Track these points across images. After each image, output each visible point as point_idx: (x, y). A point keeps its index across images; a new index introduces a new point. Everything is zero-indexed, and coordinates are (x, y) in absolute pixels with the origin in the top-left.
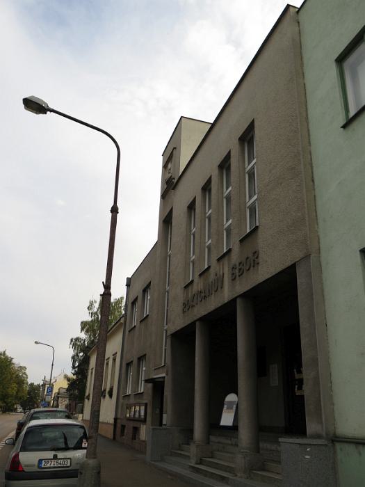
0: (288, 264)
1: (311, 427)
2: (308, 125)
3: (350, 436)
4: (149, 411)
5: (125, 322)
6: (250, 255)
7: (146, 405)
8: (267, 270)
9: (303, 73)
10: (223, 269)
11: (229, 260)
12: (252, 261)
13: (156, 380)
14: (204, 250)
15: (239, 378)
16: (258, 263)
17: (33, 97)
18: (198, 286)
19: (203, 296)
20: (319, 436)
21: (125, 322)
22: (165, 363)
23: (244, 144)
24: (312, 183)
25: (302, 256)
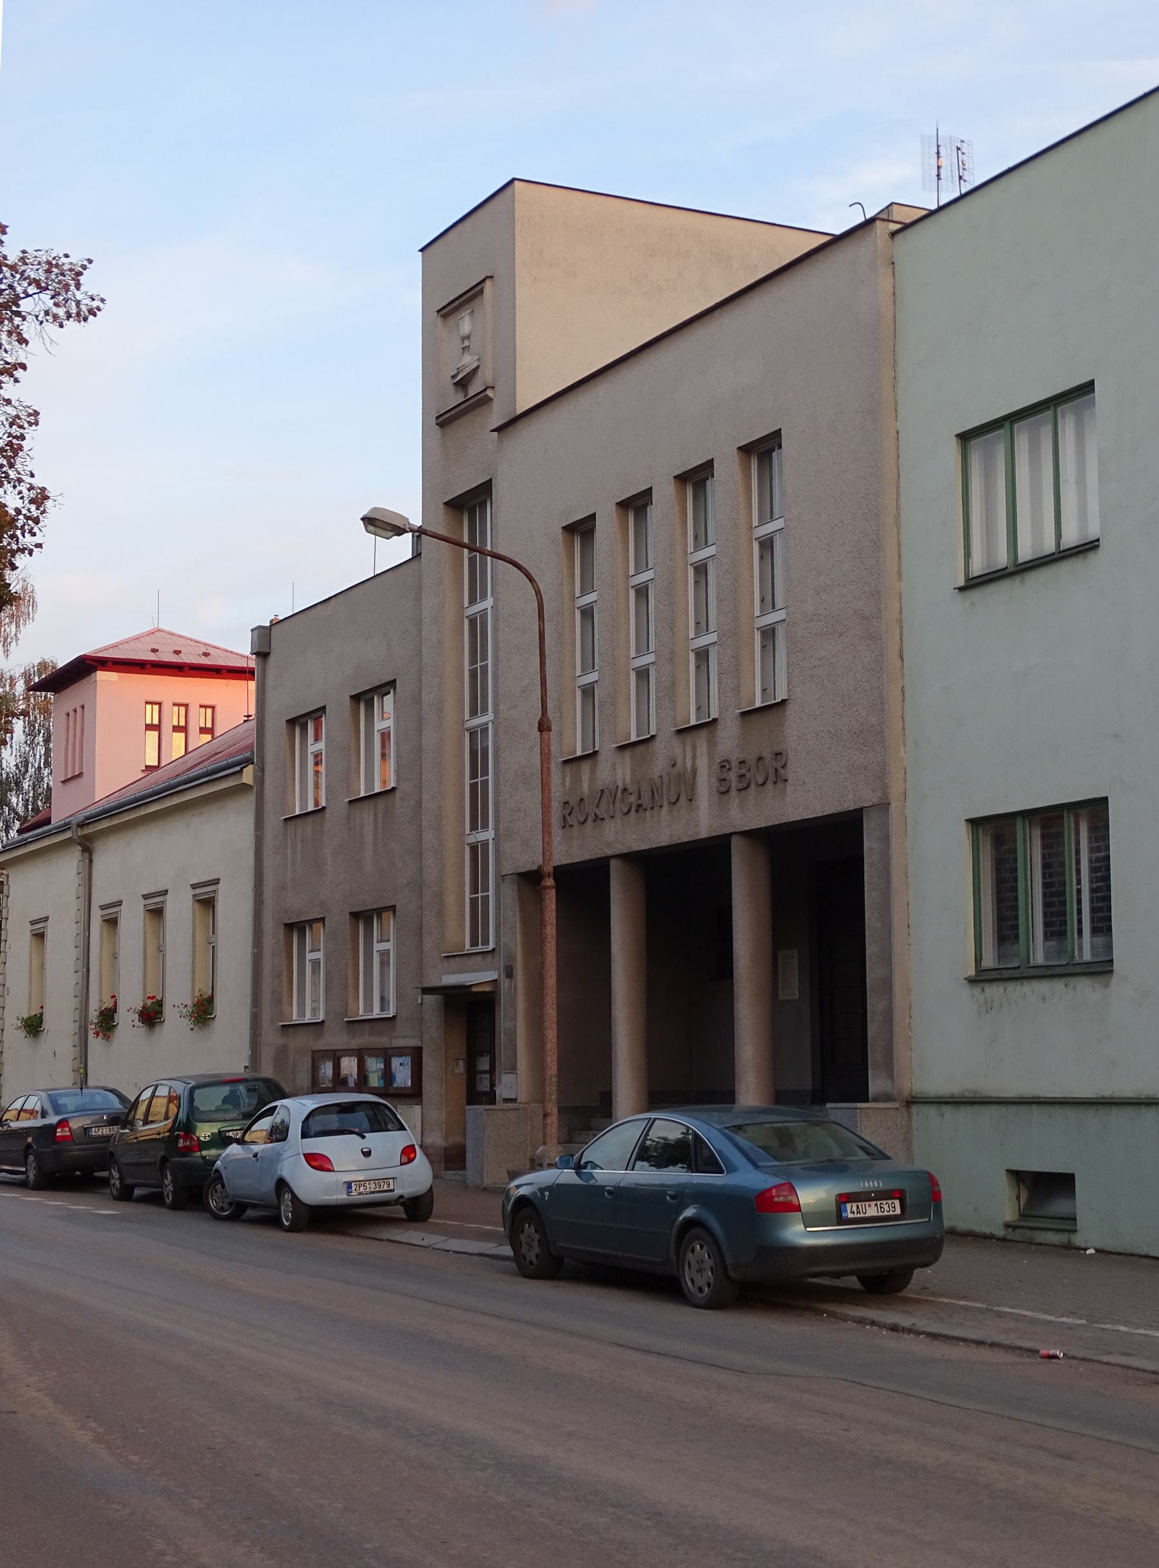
0: (849, 804)
1: (876, 1084)
2: (898, 533)
3: (932, 1094)
4: (430, 1066)
5: (260, 779)
6: (767, 755)
7: (416, 1055)
8: (805, 799)
9: (896, 404)
10: (694, 758)
11: (712, 744)
12: (771, 770)
13: (475, 989)
14: (628, 675)
15: (612, 905)
16: (786, 780)
17: (375, 510)
18: (615, 771)
19: (640, 802)
20: (888, 1098)
21: (260, 779)
22: (497, 941)
23: (749, 461)
24: (899, 661)
25: (875, 801)
